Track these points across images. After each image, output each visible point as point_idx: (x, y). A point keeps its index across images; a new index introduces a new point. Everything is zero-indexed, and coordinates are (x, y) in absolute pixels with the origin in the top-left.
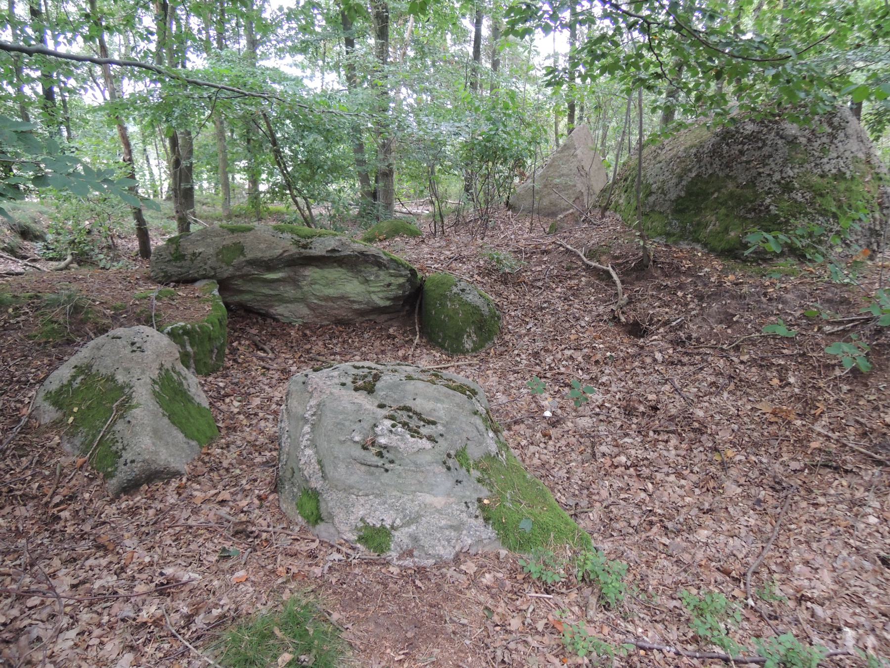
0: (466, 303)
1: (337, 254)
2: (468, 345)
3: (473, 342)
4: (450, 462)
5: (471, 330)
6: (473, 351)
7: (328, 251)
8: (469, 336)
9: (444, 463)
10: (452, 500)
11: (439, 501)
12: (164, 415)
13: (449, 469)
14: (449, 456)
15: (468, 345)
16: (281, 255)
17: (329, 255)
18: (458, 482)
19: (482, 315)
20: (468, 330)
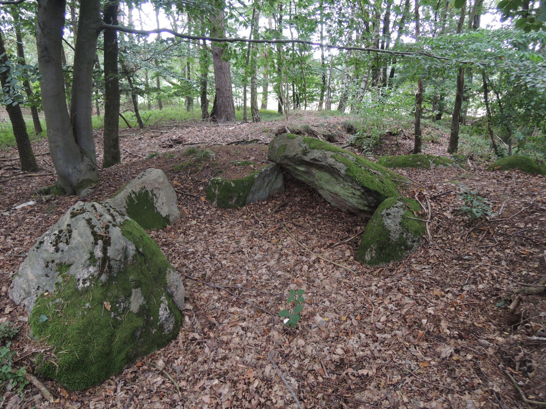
0: (383, 226)
1: (318, 163)
2: (368, 258)
3: (372, 257)
4: (50, 265)
5: (374, 246)
6: (369, 264)
7: (311, 159)
8: (371, 251)
9: (48, 262)
10: (35, 280)
11: (31, 276)
12: (125, 207)
13: (47, 266)
14: (53, 261)
15: (368, 258)
16: (295, 156)
17: (312, 162)
18: (47, 275)
19: (389, 239)
20: (372, 246)
